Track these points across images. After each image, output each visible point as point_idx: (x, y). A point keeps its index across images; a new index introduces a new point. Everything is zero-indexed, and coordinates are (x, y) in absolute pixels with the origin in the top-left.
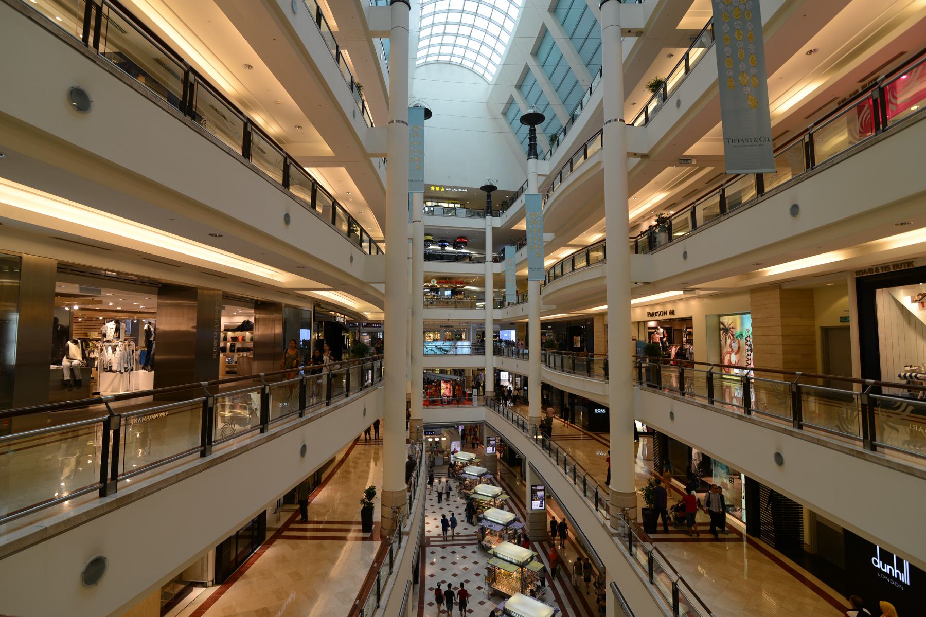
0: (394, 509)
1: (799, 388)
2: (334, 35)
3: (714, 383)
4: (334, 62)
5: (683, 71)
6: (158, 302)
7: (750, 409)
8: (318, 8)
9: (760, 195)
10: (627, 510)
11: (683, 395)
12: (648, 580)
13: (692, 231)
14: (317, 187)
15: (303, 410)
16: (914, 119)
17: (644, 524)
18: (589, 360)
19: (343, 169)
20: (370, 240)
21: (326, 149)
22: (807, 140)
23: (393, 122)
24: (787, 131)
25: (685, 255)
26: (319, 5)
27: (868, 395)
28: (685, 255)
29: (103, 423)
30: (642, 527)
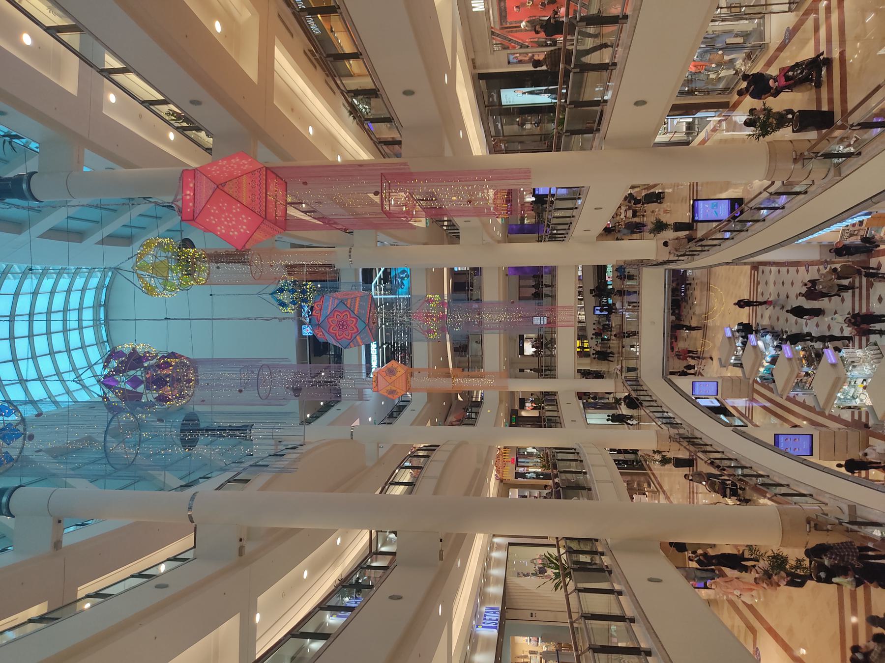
0: (810, 528)
1: (567, 131)
2: (53, 609)
3: (589, 62)
4: (110, 602)
5: (132, 76)
6: (563, 151)
7: (621, 17)
8: (132, 576)
9: (360, 56)
10: (796, 155)
11: (626, 17)
12: (856, 159)
13: (363, 59)
14: (325, 605)
15: (641, 650)
16: (335, 2)
17: (819, 128)
18: (576, 66)
19: (260, 599)
20: (362, 568)
21: (231, 627)
22: (331, 59)
23: (190, 517)
24: (279, 15)
25: (408, 93)
26: (26, 620)
27: (578, 22)
28: (408, 93)
29: (596, 654)
30: (824, 131)
